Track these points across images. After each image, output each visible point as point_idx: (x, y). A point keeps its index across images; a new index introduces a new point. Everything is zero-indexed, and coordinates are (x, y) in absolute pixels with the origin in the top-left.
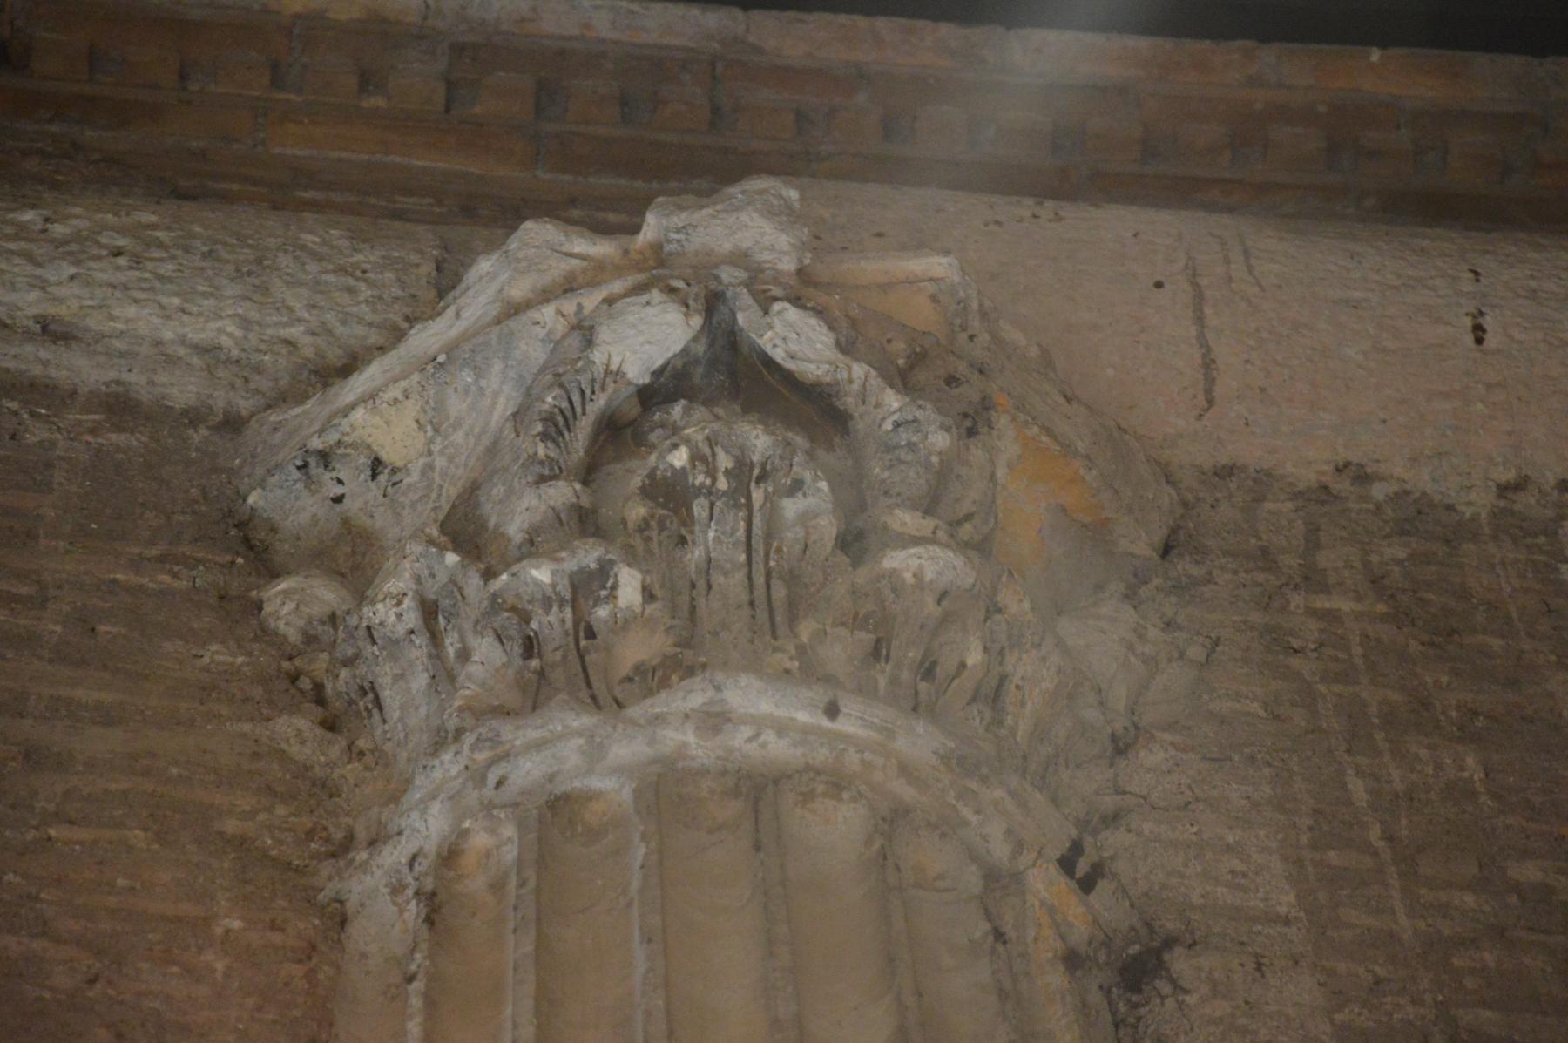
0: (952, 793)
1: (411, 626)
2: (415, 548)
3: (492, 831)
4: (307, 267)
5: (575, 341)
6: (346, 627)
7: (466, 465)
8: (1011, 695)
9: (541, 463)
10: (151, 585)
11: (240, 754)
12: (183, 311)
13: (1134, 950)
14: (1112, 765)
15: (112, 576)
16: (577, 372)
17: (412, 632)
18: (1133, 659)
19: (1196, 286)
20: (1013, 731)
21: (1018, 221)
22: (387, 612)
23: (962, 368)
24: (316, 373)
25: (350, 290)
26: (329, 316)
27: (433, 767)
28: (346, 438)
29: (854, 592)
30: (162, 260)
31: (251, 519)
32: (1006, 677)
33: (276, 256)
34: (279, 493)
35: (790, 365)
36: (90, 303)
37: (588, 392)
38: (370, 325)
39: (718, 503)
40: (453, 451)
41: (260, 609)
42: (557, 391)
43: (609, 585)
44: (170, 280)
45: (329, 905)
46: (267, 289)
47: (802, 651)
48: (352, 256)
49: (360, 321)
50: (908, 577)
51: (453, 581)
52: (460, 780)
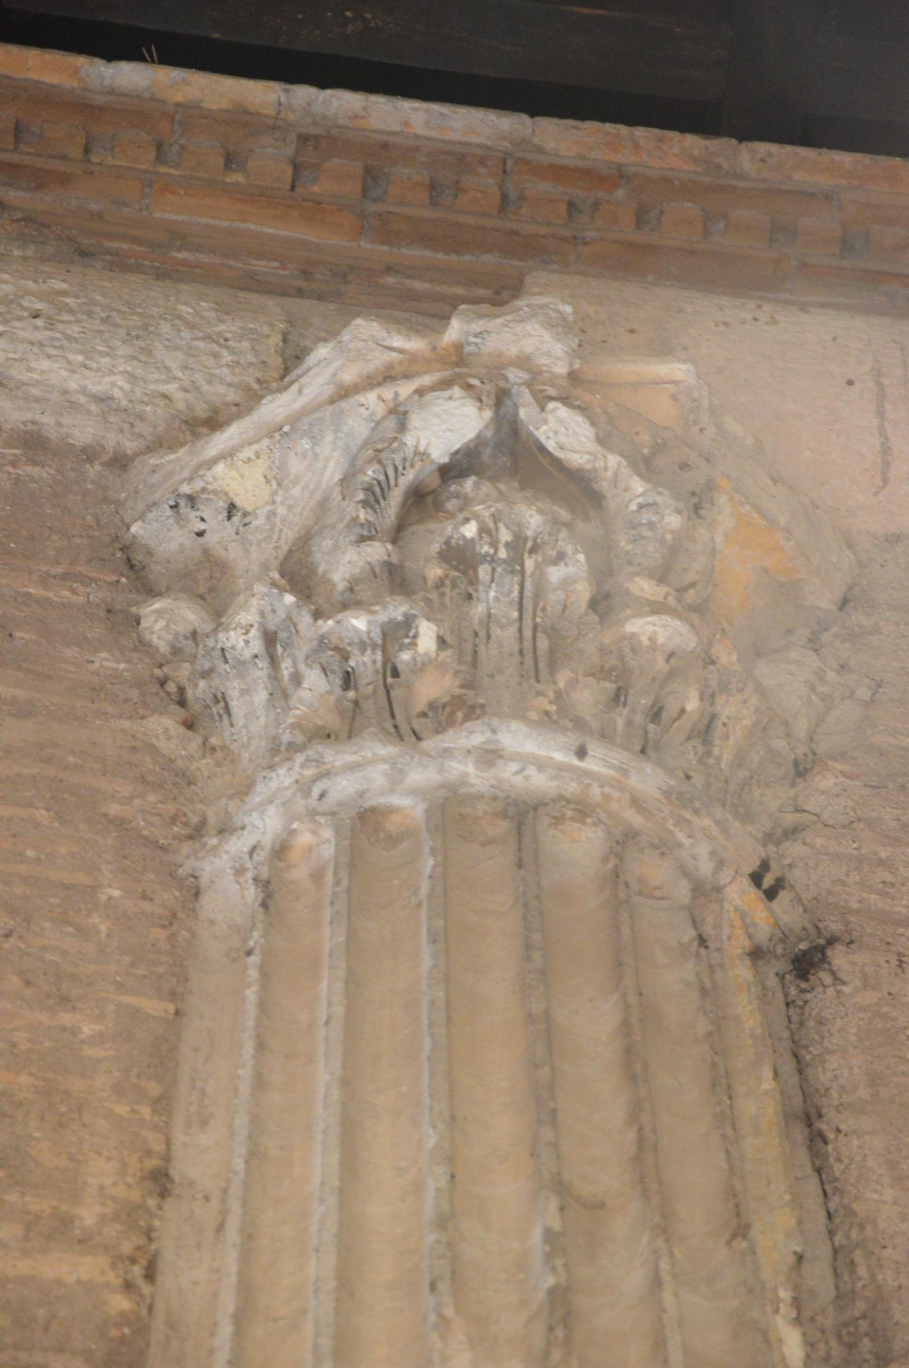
0: (671, 821)
1: (255, 651)
2: (260, 588)
3: (315, 833)
4: (182, 334)
5: (391, 423)
6: (205, 646)
7: (301, 515)
8: (718, 730)
9: (362, 525)
10: (56, 599)
11: (121, 747)
12: (86, 367)
13: (803, 946)
14: (793, 785)
15: (26, 589)
16: (393, 451)
17: (256, 656)
18: (814, 698)
19: (879, 384)
20: (718, 759)
21: (742, 323)
22: (237, 639)
23: (693, 458)
24: (186, 422)
25: (215, 356)
26: (197, 376)
27: (271, 778)
28: (209, 486)
29: (603, 651)
30: (69, 322)
31: (133, 543)
32: (715, 715)
33: (158, 324)
34: (155, 525)
35: (559, 454)
36: (14, 356)
37: (400, 468)
38: (229, 385)
39: (499, 569)
40: (291, 502)
41: (138, 624)
42: (376, 466)
43: (411, 634)
44: (76, 340)
45: (186, 879)
46: (151, 351)
47: (558, 694)
48: (217, 326)
49: (222, 380)
50: (645, 640)
51: (289, 618)
52: (291, 791)
